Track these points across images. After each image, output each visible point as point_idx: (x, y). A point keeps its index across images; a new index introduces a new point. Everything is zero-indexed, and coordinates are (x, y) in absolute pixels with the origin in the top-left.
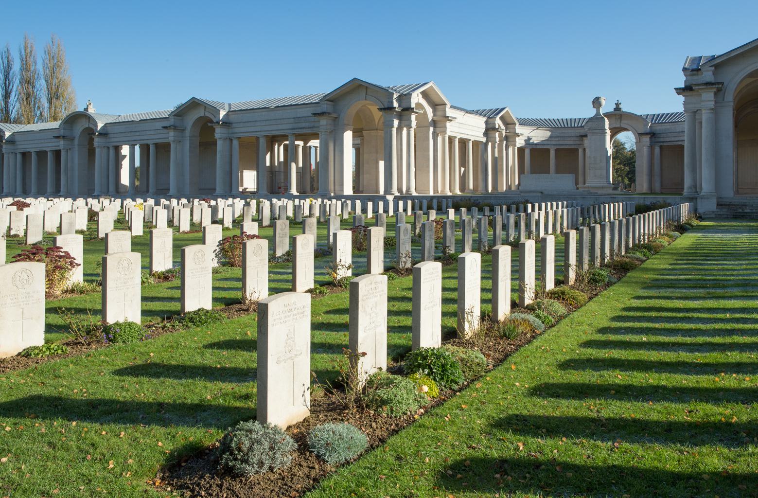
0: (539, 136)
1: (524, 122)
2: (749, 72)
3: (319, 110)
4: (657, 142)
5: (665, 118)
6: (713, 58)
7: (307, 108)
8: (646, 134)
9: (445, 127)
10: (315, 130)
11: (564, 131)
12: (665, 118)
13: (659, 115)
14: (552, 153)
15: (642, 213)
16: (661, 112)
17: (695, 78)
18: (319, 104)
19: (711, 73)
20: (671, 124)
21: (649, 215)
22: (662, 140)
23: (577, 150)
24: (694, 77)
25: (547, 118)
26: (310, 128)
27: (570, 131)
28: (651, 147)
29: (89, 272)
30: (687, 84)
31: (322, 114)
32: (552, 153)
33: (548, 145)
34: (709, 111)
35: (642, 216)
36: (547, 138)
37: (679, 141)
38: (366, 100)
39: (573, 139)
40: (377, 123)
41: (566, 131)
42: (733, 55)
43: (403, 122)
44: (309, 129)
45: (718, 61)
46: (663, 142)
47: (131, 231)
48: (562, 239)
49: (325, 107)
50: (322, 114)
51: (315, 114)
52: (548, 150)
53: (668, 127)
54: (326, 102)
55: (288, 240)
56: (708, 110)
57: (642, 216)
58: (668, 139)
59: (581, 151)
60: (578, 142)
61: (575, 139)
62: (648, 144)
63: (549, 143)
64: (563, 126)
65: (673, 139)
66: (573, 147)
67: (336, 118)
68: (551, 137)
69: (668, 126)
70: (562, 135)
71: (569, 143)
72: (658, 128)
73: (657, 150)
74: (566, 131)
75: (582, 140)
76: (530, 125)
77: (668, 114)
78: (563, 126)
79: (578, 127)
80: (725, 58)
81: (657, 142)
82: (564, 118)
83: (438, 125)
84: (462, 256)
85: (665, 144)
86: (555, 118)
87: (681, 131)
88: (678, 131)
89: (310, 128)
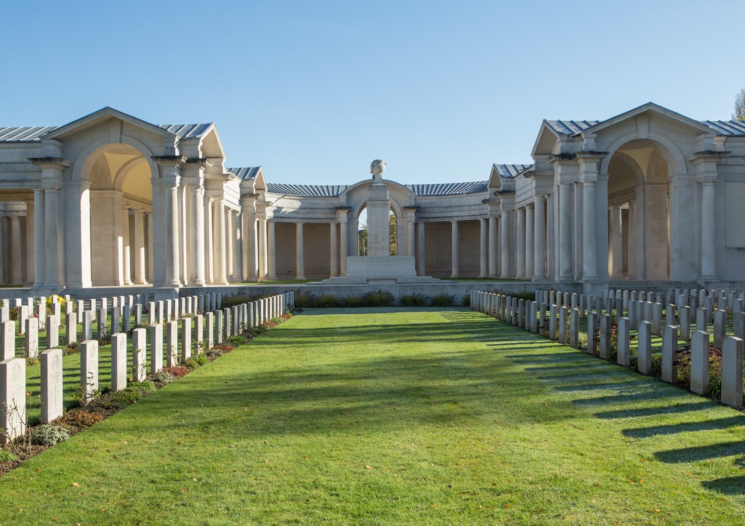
0: (290, 205)
1: (274, 189)
2: (623, 143)
3: (38, 153)
4: (421, 218)
5: (449, 188)
6: (598, 123)
7: (10, 148)
8: (412, 208)
9: (221, 189)
10: (27, 186)
11: (313, 201)
12: (449, 188)
13: (443, 185)
14: (299, 229)
15: (267, 297)
16: (446, 182)
17: (571, 144)
18: (38, 145)
19: (593, 141)
20: (437, 197)
21: (277, 297)
22: (427, 215)
23: (328, 225)
24: (570, 143)
25: (308, 185)
26: (18, 181)
27: (320, 202)
28: (416, 225)
29: (67, 367)
30: (564, 151)
31: (48, 159)
32: (299, 229)
33: (295, 218)
34: (591, 184)
35: (275, 297)
36: (294, 210)
37: (446, 217)
38: (120, 142)
39: (324, 211)
40: (113, 179)
41: (316, 202)
42: (615, 122)
43: (186, 179)
44: (17, 184)
45: (600, 127)
46: (428, 218)
47: (38, 317)
48: (81, 326)
49: (52, 149)
50: (48, 159)
51: (34, 160)
52: (294, 225)
53: (434, 201)
54: (53, 141)
55: (76, 328)
56: (591, 182)
57: (275, 297)
58: (433, 215)
59: (333, 227)
60: (331, 216)
61: (327, 211)
62: (413, 219)
63: (296, 215)
64: (323, 195)
65: (439, 215)
66: (324, 221)
67: (67, 167)
68: (301, 208)
69: (433, 200)
70: (311, 206)
71: (319, 216)
72: (423, 201)
73: (421, 227)
74: (316, 202)
75: (335, 213)
76: (277, 193)
77: (448, 185)
78: (327, 195)
79: (434, 195)
80: (608, 125)
81: (421, 218)
82: (330, 184)
83: (210, 187)
84: (83, 343)
85: (431, 220)
86: (319, 185)
87: (448, 205)
88: (445, 205)
89: (18, 181)
